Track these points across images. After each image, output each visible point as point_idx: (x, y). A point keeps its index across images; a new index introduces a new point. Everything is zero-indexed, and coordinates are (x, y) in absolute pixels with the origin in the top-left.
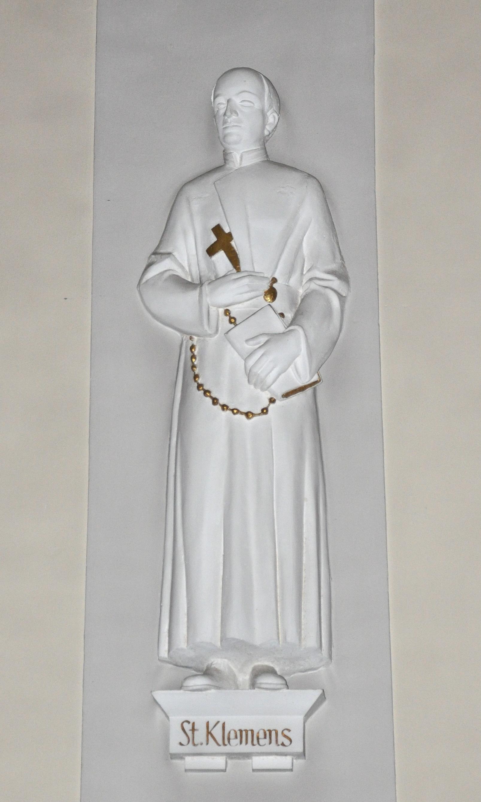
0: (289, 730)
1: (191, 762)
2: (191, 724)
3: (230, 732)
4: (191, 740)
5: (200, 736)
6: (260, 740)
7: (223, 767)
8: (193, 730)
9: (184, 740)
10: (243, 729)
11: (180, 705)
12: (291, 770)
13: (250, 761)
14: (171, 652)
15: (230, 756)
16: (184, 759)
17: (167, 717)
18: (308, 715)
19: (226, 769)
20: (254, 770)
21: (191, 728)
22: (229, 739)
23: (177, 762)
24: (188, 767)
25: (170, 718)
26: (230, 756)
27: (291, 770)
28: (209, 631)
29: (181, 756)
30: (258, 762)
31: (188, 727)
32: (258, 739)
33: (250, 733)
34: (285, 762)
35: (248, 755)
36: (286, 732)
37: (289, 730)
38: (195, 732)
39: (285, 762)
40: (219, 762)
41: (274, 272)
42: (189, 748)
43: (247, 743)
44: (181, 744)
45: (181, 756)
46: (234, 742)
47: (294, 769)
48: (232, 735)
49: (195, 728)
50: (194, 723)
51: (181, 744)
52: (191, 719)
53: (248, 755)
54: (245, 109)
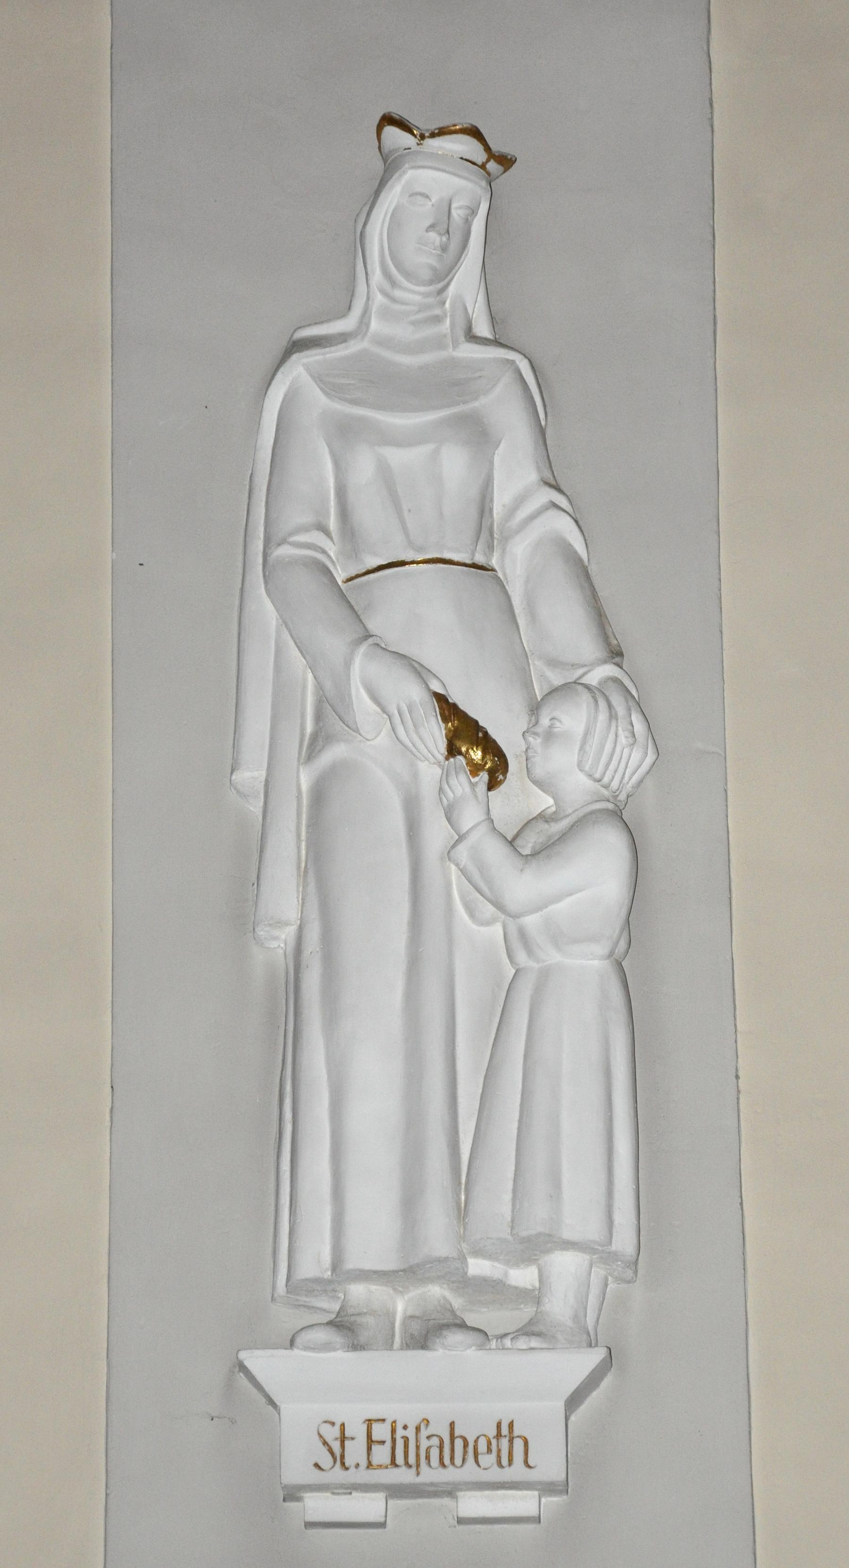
1: (318, 1506)
2: (337, 1427)
3: (476, 1441)
4: (341, 1461)
5: (355, 1451)
6: (480, 1457)
7: (382, 1520)
8: (343, 1439)
9: (326, 1460)
11: (317, 1388)
14: (290, 1283)
15: (395, 1491)
16: (299, 1499)
18: (573, 1401)
19: (386, 1521)
24: (310, 1518)
25: (283, 1407)
26: (395, 1491)
28: (374, 1239)
30: (473, 1504)
31: (331, 1434)
34: (523, 1503)
35: (451, 1491)
38: (347, 1443)
39: (523, 1503)
40: (370, 1507)
41: (473, 555)
42: (337, 1475)
43: (442, 1464)
44: (317, 1465)
45: (293, 1494)
46: (488, 1460)
48: (482, 1446)
49: (347, 1434)
50: (343, 1425)
51: (317, 1465)
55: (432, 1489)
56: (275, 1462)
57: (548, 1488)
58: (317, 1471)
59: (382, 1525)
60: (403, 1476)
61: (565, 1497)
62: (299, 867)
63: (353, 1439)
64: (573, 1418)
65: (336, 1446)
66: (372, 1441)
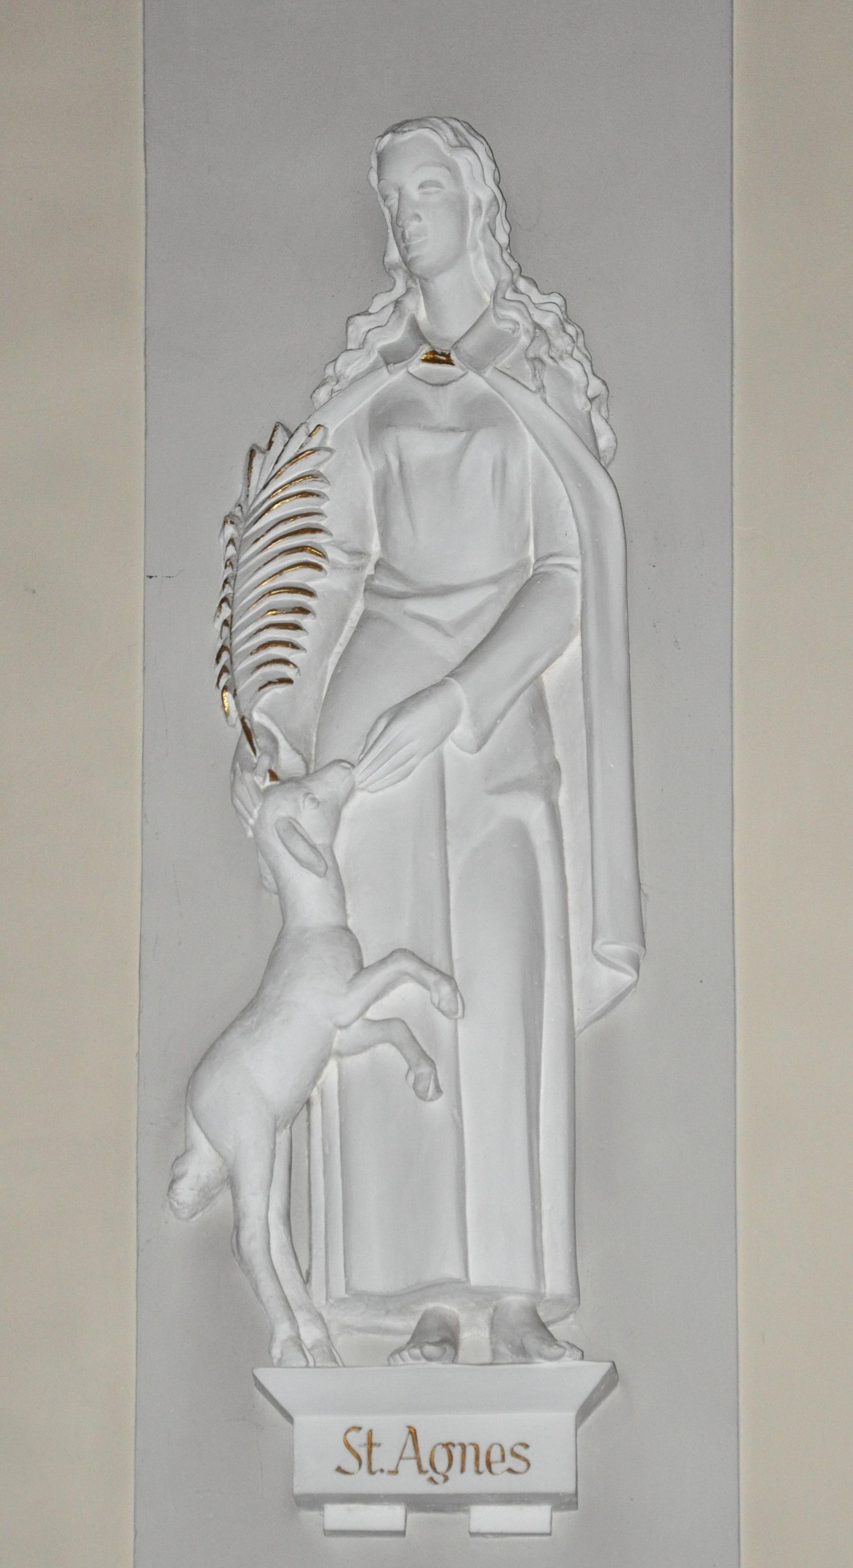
0: (526, 1446)
1: (337, 1516)
3: (488, 1453)
5: (383, 1458)
7: (546, 1529)
8: (370, 1445)
9: (350, 1464)
10: (466, 1441)
12: (550, 1534)
13: (461, 1515)
16: (321, 1508)
17: (289, 1418)
18: (584, 1412)
20: (473, 1534)
21: (364, 1440)
22: (489, 1464)
23: (308, 1515)
26: (414, 1503)
27: (550, 1534)
29: (316, 1502)
30: (484, 1517)
31: (358, 1440)
32: (489, 1464)
33: (470, 1451)
36: (520, 1450)
37: (526, 1446)
38: (374, 1449)
44: (339, 1470)
45: (316, 1502)
47: (553, 1534)
48: (496, 1455)
51: (339, 1470)
52: (367, 1421)
53: (460, 1503)
54: (441, 188)
55: (538, 1229)
56: (288, 1466)
57: (563, 1502)
58: (339, 1475)
59: (402, 1533)
60: (419, 1485)
61: (573, 1512)
62: (369, 735)
63: (379, 1445)
64: (580, 1431)
65: (363, 1453)
66: (415, 1458)
